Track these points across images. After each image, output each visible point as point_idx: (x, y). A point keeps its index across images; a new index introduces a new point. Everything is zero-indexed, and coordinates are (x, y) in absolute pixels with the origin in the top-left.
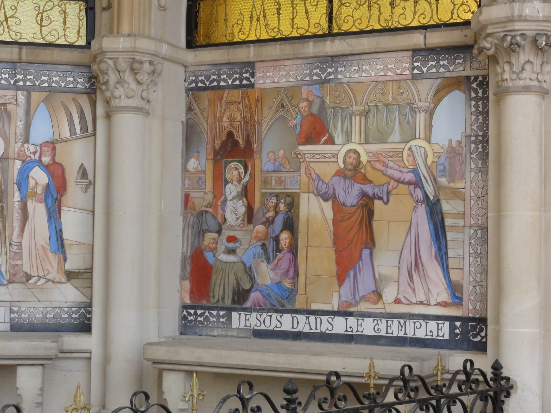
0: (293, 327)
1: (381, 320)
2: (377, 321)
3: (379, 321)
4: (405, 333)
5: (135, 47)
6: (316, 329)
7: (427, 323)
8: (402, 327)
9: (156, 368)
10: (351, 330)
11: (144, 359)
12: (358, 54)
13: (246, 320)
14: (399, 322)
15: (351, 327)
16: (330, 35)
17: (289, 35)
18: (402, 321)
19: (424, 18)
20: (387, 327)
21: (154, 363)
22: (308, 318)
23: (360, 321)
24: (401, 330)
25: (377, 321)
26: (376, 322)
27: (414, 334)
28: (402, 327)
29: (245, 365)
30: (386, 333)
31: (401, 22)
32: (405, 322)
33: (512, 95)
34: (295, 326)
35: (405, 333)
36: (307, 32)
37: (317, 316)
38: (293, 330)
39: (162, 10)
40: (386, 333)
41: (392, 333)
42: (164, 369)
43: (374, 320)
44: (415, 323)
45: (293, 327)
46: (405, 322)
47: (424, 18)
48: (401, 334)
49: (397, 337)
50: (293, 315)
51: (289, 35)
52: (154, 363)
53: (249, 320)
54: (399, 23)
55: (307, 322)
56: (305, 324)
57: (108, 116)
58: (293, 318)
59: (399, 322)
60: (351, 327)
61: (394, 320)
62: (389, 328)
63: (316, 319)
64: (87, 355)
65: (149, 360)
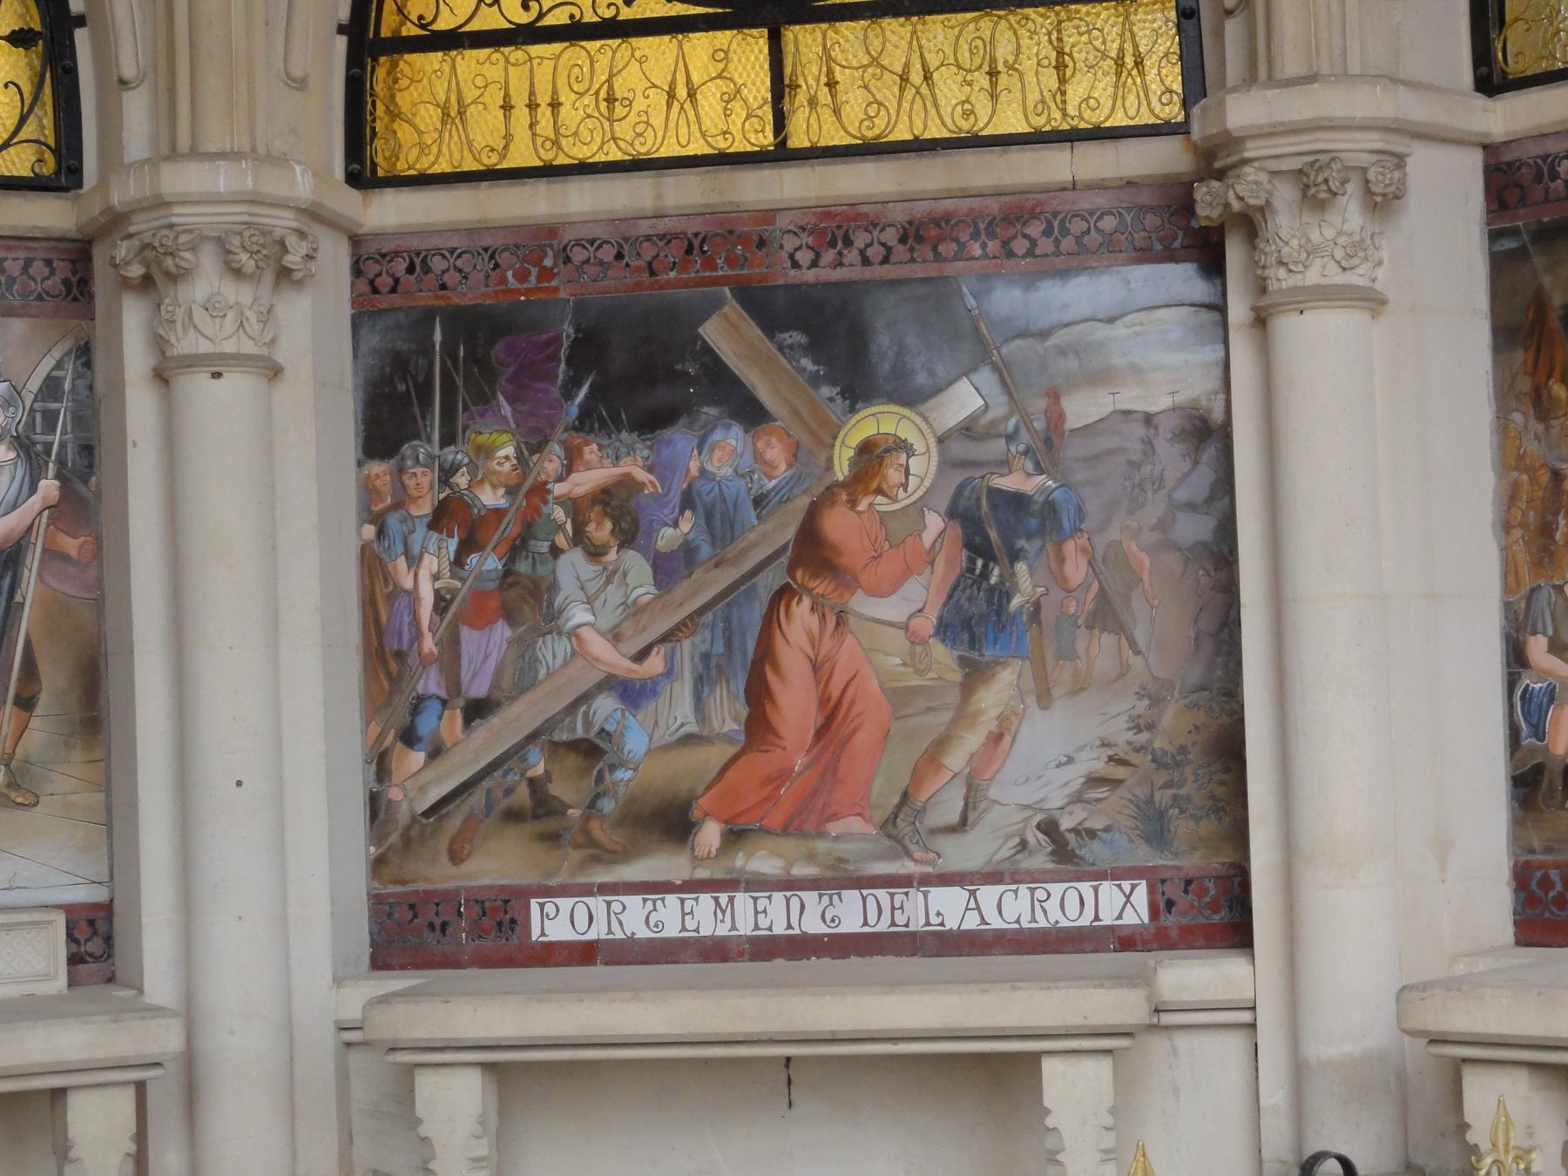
0: (866, 924)
1: (663, 900)
2: (654, 902)
3: (835, 898)
4: (734, 928)
5: (160, 195)
6: (789, 926)
7: (926, 895)
8: (724, 912)
9: (1442, 1056)
10: (939, 920)
11: (1404, 1031)
12: (913, 200)
13: (756, 912)
14: (716, 900)
15: (938, 914)
16: (781, 154)
17: (590, 157)
18: (724, 898)
19: (641, 144)
20: (684, 914)
21: (1435, 1041)
22: (973, 893)
23: (762, 904)
24: (722, 921)
25: (654, 902)
26: (649, 905)
27: (1097, 918)
28: (724, 912)
29: (1004, 1029)
30: (787, 929)
31: (1086, 116)
32: (731, 900)
33: (194, 373)
34: (872, 919)
35: (734, 928)
36: (409, 168)
37: (788, 894)
38: (866, 929)
39: (292, 87)
40: (787, 929)
41: (907, 925)
42: (1465, 1060)
43: (645, 901)
44: (609, 904)
45: (866, 924)
46: (731, 900)
47: (641, 144)
48: (723, 930)
49: (712, 937)
50: (865, 892)
51: (590, 157)
52: (1432, 1041)
53: (765, 911)
54: (1081, 118)
55: (972, 904)
56: (967, 909)
57: (1261, 321)
58: (864, 899)
59: (716, 900)
60: (938, 914)
61: (774, 893)
62: (761, 916)
63: (788, 900)
64: (1245, 1017)
65: (1414, 1034)
